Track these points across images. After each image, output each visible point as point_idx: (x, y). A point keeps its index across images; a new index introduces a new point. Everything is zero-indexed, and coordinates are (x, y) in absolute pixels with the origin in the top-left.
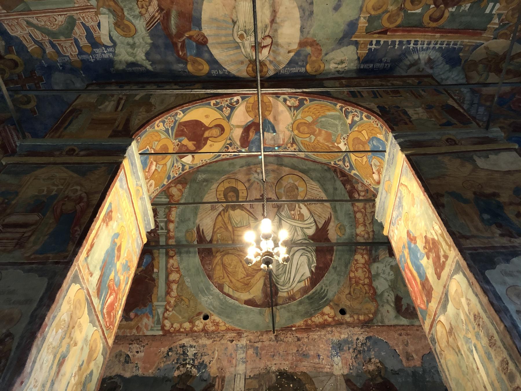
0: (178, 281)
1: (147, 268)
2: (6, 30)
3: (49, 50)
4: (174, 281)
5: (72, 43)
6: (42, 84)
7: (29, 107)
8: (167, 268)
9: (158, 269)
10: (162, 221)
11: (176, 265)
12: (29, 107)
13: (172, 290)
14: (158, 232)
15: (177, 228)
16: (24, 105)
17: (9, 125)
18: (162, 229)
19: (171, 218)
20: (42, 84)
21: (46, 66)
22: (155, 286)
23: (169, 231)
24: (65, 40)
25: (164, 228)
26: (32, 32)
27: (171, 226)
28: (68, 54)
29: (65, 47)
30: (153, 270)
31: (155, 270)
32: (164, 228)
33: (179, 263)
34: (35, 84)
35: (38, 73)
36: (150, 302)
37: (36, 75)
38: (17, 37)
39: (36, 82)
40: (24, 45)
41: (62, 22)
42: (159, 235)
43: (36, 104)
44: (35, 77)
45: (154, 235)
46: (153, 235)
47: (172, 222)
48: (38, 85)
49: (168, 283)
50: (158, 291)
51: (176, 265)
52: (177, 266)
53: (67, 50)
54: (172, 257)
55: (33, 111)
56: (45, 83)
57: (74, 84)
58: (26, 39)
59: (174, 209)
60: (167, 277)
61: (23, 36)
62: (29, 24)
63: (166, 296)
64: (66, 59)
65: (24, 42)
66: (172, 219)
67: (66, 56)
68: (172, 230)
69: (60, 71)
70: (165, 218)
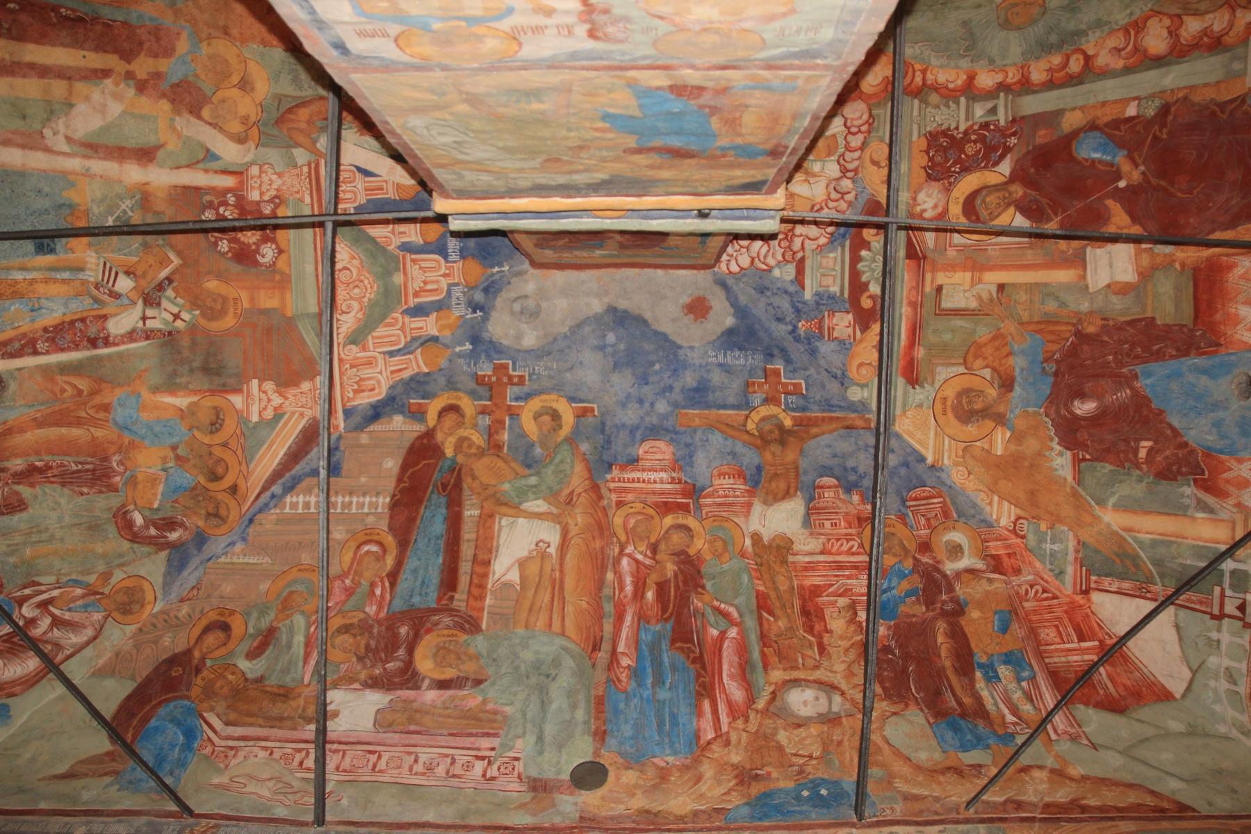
0: (1171, 16)
1: (1121, 145)
2: (370, 404)
3: (429, 325)
4: (1173, 33)
5: (412, 260)
6: (514, 370)
7: (568, 418)
8: (1127, 70)
9: (1125, 102)
10: (969, 113)
11: (1116, 41)
12: (568, 418)
13: (1205, 32)
14: (1002, 123)
15: (992, 61)
16: (560, 427)
17: (609, 476)
18: (993, 111)
19: (959, 82)
20: (514, 370)
21: (468, 346)
22: (1185, 98)
23: (1002, 87)
24: (405, 274)
25: (990, 105)
26: (382, 344)
27: (986, 80)
28: (444, 283)
29: (425, 283)
30: (1131, 119)
31: (1131, 111)
32: (990, 105)
33: (1110, 33)
34: (512, 384)
35: (486, 369)
36: (1243, 102)
37: (489, 377)
38: (392, 387)
39: (505, 380)
40: (412, 379)
41: (353, 258)
42: (1014, 120)
43: (564, 400)
44: (494, 379)
45: (1014, 134)
46: (1014, 140)
47: (971, 78)
48: (516, 380)
49: (1179, 52)
50: (1206, 85)
51: (1116, 41)
52: (1121, 34)
53: (432, 282)
54: (1088, 58)
55: (583, 413)
56: (514, 364)
57: (526, 297)
58: (400, 370)
59: (930, 77)
60: (1159, 61)
61: (392, 372)
62: (356, 339)
63: (1227, 48)
64: (457, 292)
65: (406, 375)
66: (960, 81)
67: (449, 291)
68: (999, 78)
69: (485, 319)
70: (958, 104)
